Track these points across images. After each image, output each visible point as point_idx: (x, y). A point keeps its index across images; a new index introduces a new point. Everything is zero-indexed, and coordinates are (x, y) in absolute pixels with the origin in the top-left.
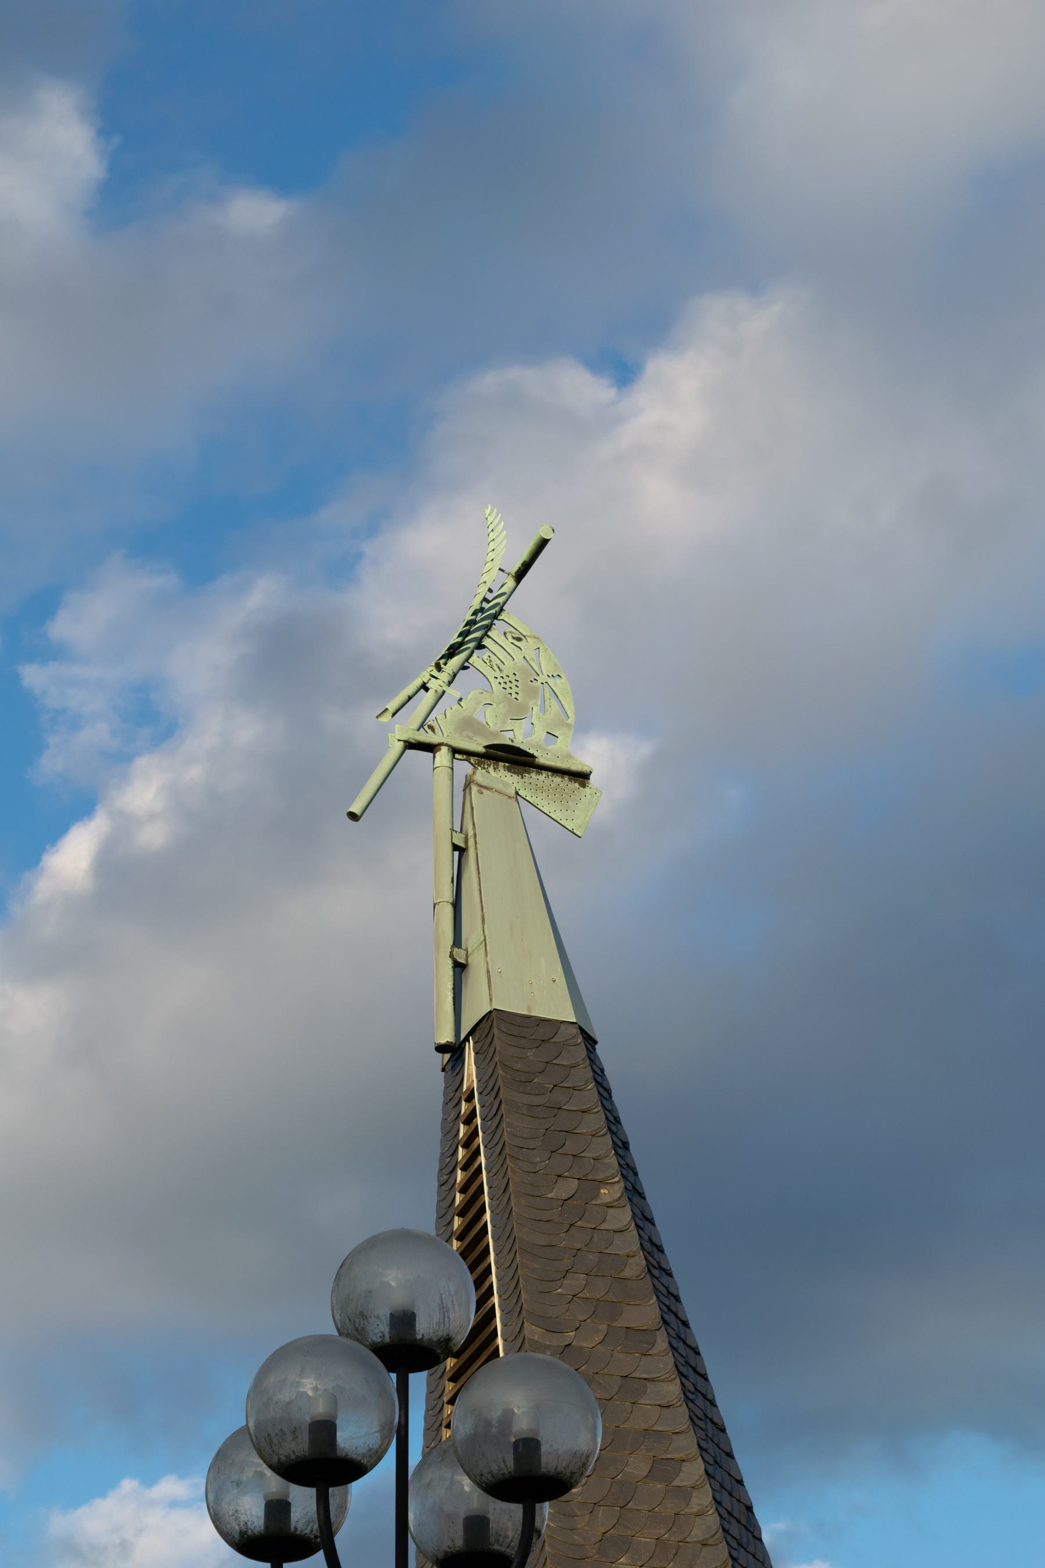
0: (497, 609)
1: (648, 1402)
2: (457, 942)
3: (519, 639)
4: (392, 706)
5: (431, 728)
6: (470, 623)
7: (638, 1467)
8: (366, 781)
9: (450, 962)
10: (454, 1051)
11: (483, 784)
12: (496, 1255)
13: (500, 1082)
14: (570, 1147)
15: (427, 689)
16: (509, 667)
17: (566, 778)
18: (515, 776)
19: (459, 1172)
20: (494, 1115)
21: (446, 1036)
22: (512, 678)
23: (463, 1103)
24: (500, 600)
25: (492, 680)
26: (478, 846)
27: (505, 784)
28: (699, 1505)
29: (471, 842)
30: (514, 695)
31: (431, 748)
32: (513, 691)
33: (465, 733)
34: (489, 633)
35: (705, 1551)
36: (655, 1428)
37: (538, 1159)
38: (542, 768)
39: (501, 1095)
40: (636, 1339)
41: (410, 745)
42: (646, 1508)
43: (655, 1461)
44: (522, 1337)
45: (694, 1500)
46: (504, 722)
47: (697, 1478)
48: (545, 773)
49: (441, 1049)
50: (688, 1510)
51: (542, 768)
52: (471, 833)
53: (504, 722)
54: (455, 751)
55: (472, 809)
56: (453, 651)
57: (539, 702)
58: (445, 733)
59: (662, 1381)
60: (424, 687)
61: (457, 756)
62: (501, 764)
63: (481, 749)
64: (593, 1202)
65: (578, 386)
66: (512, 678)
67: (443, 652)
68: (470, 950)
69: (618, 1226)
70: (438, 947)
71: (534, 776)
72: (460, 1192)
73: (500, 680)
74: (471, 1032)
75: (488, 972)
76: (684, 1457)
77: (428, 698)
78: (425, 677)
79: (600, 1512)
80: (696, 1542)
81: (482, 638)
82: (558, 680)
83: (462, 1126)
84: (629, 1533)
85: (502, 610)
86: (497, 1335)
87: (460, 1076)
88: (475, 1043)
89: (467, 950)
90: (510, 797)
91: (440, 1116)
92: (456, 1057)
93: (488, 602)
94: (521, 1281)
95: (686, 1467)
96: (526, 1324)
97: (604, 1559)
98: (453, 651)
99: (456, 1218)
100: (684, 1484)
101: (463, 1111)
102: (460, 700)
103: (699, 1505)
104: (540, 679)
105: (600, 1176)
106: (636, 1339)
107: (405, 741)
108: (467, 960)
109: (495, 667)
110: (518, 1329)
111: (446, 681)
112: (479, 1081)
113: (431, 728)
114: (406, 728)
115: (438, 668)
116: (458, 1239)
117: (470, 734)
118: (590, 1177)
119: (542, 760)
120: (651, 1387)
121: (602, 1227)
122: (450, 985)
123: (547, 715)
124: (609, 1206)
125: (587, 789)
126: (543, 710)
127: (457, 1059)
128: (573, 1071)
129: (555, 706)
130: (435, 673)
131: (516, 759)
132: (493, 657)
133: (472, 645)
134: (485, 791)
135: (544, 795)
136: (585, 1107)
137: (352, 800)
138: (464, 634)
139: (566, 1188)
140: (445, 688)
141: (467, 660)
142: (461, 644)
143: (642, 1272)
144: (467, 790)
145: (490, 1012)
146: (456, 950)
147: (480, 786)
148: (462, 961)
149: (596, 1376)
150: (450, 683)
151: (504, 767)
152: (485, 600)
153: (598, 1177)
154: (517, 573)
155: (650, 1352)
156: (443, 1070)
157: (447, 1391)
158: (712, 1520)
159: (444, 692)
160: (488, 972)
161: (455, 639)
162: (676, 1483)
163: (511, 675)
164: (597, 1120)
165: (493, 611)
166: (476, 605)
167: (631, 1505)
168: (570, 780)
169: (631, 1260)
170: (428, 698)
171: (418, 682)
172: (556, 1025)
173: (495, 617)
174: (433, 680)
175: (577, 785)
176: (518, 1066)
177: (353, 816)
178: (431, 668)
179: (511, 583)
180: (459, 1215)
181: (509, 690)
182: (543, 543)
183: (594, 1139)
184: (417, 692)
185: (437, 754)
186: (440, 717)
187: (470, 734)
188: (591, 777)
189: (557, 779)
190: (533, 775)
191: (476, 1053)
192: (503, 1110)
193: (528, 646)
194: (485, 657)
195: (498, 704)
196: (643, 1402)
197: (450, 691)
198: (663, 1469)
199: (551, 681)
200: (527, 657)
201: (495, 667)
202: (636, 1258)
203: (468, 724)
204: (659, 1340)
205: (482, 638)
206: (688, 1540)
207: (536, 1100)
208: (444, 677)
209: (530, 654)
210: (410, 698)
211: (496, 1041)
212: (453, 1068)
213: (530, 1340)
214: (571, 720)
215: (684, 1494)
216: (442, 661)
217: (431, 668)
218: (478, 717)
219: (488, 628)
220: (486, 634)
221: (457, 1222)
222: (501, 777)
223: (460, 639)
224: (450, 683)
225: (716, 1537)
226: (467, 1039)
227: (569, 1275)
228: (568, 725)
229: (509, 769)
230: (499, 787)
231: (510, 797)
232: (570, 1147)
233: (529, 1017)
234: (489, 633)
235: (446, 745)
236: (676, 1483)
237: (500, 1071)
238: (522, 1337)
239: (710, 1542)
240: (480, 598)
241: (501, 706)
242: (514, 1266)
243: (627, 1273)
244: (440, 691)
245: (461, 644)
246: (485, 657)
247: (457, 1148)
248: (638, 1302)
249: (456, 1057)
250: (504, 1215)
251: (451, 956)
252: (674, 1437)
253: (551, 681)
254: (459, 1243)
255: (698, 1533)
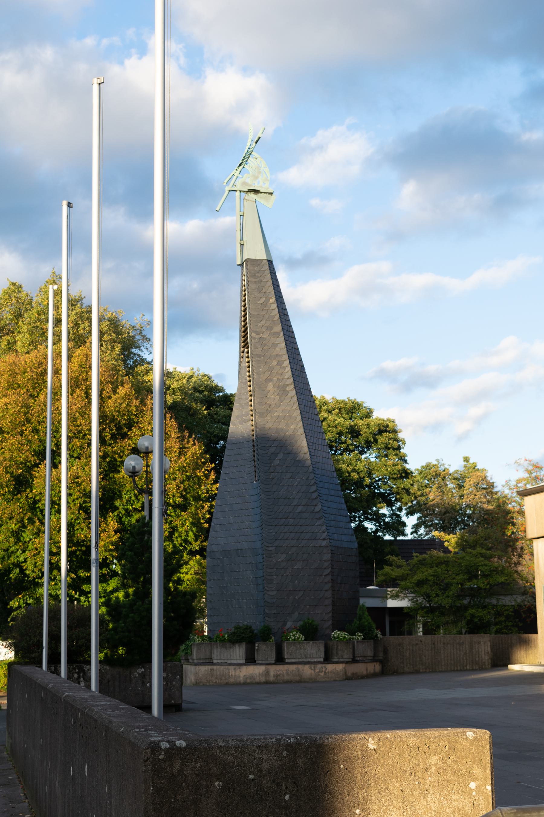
7: (275, 363)
10: (242, 265)
21: (239, 263)
38: (261, 192)
40: (276, 334)
41: (230, 191)
51: (261, 192)
54: (240, 191)
56: (240, 165)
58: (239, 187)
77: (234, 178)
78: (233, 173)
79: (266, 373)
95: (285, 362)
98: (240, 165)
106: (276, 334)
119: (261, 191)
124: (272, 304)
139: (263, 300)
152: (249, 148)
158: (290, 373)
161: (241, 162)
164: (270, 283)
171: (232, 174)
172: (262, 260)
173: (250, 154)
179: (254, 144)
182: (260, 138)
198: (280, 363)
203: (244, 183)
208: (238, 172)
215: (284, 368)
218: (246, 181)
222: (252, 196)
230: (251, 199)
241: (173, 420)
243: (275, 319)
250: (249, 308)
255: (287, 377)
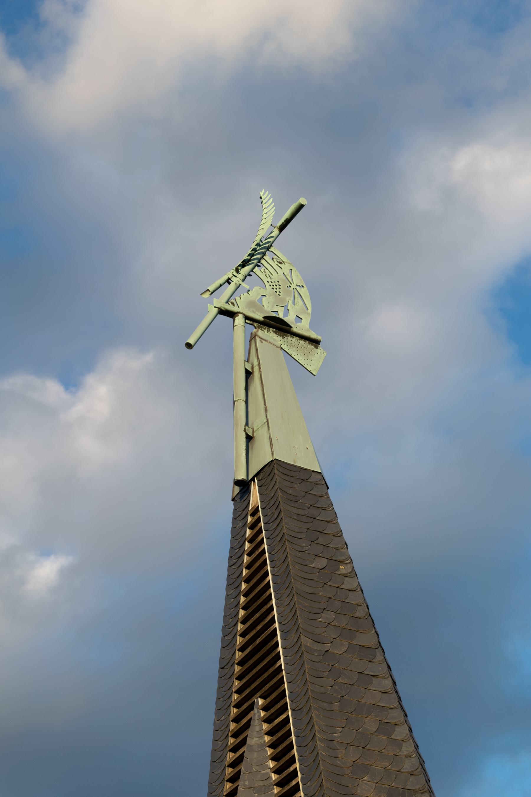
0: (269, 244)
1: (374, 689)
2: (247, 424)
3: (281, 263)
4: (211, 288)
5: (232, 303)
6: (254, 250)
8: (196, 328)
9: (244, 434)
10: (243, 485)
11: (263, 338)
12: (277, 599)
13: (280, 499)
14: (321, 540)
15: (229, 283)
16: (275, 278)
17: (307, 342)
18: (279, 337)
19: (246, 556)
20: (275, 520)
21: (242, 476)
22: (277, 284)
23: (249, 516)
24: (271, 240)
25: (266, 283)
26: (262, 370)
27: (275, 340)
28: (407, 751)
29: (256, 369)
30: (278, 293)
31: (232, 315)
32: (278, 290)
33: (251, 309)
34: (264, 257)
35: (412, 778)
36: (379, 704)
37: (304, 545)
39: (281, 507)
42: (377, 749)
43: (381, 723)
44: (299, 644)
45: (404, 748)
46: (273, 307)
47: (405, 735)
48: (295, 338)
49: (238, 483)
50: (400, 753)
52: (256, 363)
53: (273, 307)
54: (247, 318)
55: (257, 350)
56: (245, 264)
57: (292, 299)
58: (241, 305)
59: (381, 677)
60: (228, 281)
61: (247, 321)
62: (271, 329)
63: (261, 319)
64: (336, 573)
65: (52, 390)
66: (277, 284)
67: (240, 263)
68: (255, 429)
69: (351, 588)
70: (237, 425)
71: (289, 339)
72: (246, 568)
73: (270, 283)
74: (257, 475)
75: (270, 439)
76: (397, 723)
77: (232, 287)
80: (407, 772)
81: (260, 259)
82: (302, 288)
83: (248, 530)
84: (368, 763)
85: (271, 246)
86: (278, 646)
87: (246, 502)
88: (258, 481)
89: (253, 429)
90: (277, 347)
91: (230, 526)
92: (244, 490)
93: (260, 246)
94: (298, 612)
95: (398, 729)
96: (302, 636)
97: (355, 777)
98: (245, 264)
99: (243, 583)
100: (398, 738)
101: (249, 522)
102: (249, 291)
103: (407, 751)
104: (293, 286)
105: (340, 559)
107: (219, 308)
108: (253, 435)
109: (268, 276)
110: (295, 640)
111: (241, 279)
112: (261, 502)
113: (232, 303)
114: (220, 302)
115: (237, 271)
116: (244, 596)
117: (254, 310)
118: (334, 558)
119: (295, 329)
120: (375, 680)
121: (342, 587)
122: (244, 447)
123: (296, 306)
125: (318, 350)
126: (294, 303)
127: (244, 492)
128: (320, 499)
129: (301, 302)
130: (235, 274)
131: (279, 326)
132: (266, 271)
133: (255, 261)
134: (264, 342)
135: (295, 350)
136: (329, 519)
137: (189, 336)
138: (251, 255)
139: (321, 563)
140: (241, 282)
141: (252, 271)
142: (249, 260)
143: (366, 615)
144: (253, 341)
145: (272, 461)
146: (247, 428)
147: (261, 338)
148: (251, 434)
149: (344, 671)
150: (243, 280)
151: (273, 331)
153: (337, 559)
154: (280, 226)
155: (373, 661)
156: (233, 500)
157: (234, 685)
159: (240, 284)
160: (270, 439)
161: (246, 257)
162: (392, 737)
163: (276, 282)
165: (267, 245)
166: (253, 246)
167: (368, 747)
168: (309, 344)
169: (359, 608)
170: (232, 287)
171: (225, 278)
174: (234, 277)
175: (313, 347)
176: (290, 492)
177: (189, 346)
178: (233, 271)
179: (276, 232)
180: (245, 582)
181: (275, 290)
183: (335, 538)
184: (225, 283)
185: (237, 318)
186: (238, 298)
187: (254, 310)
188: (321, 343)
189: (302, 342)
190: (289, 338)
191: (259, 487)
192: (282, 514)
193: (286, 268)
194: (262, 270)
195: (270, 296)
196: (372, 688)
197: (243, 284)
199: (298, 288)
200: (285, 273)
201: (268, 276)
202: (362, 607)
204: (378, 654)
205: (260, 259)
206: (402, 770)
207: (301, 512)
208: (240, 276)
209: (287, 273)
210: (221, 286)
211: (276, 477)
212: (241, 498)
213: (305, 646)
214: (310, 311)
216: (239, 268)
217: (233, 271)
219: (264, 254)
220: (262, 257)
221: (244, 586)
223: (249, 257)
224: (243, 280)
225: (418, 770)
226: (253, 479)
227: (325, 612)
228: (308, 314)
229: (276, 333)
230: (272, 341)
231: (277, 347)
232: (321, 540)
233: (295, 466)
234: (264, 257)
235: (242, 313)
236: (392, 737)
237: (280, 494)
238: (299, 644)
239: (415, 773)
240: (255, 243)
242: (292, 604)
243: (357, 614)
244: (238, 283)
245: (249, 260)
246: (262, 270)
247: (244, 542)
248: (365, 632)
249: (244, 490)
251: (245, 430)
252: (390, 710)
253: (298, 288)
254: (245, 598)
